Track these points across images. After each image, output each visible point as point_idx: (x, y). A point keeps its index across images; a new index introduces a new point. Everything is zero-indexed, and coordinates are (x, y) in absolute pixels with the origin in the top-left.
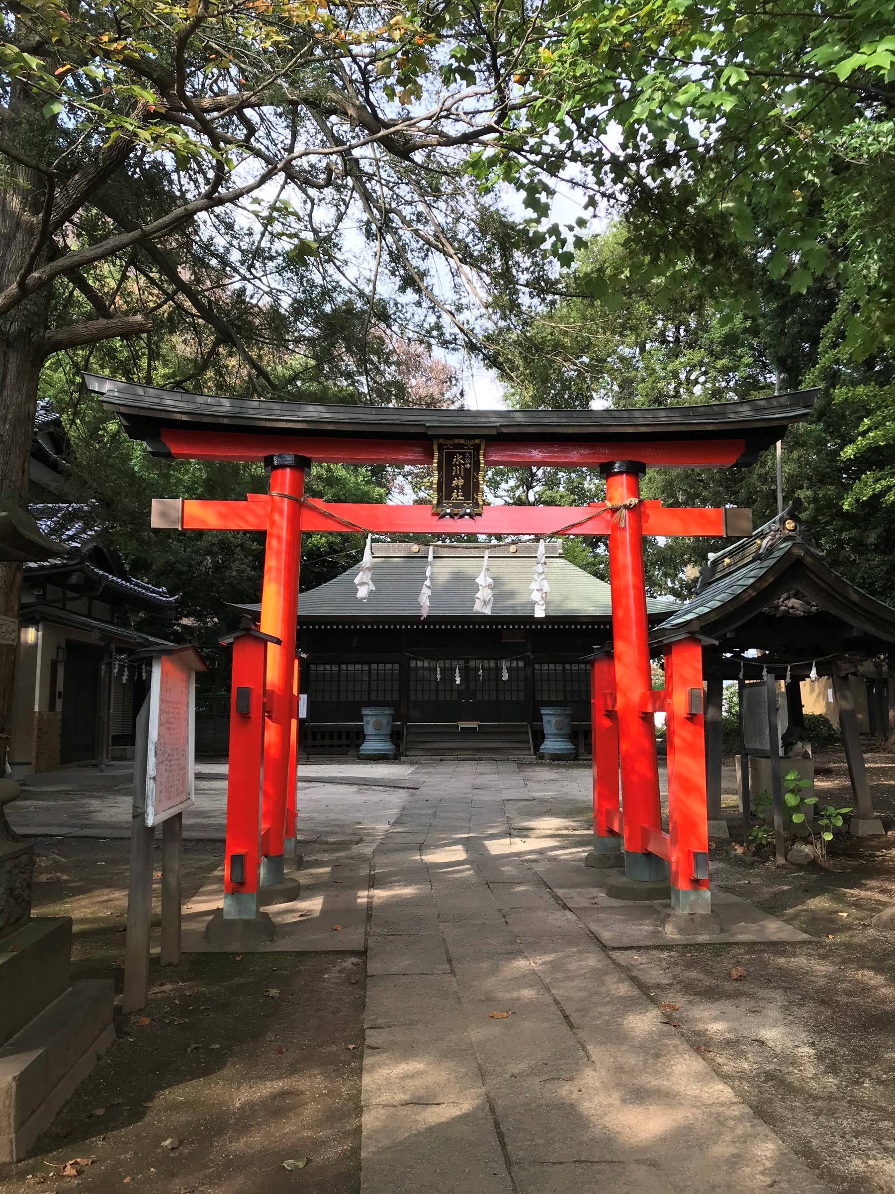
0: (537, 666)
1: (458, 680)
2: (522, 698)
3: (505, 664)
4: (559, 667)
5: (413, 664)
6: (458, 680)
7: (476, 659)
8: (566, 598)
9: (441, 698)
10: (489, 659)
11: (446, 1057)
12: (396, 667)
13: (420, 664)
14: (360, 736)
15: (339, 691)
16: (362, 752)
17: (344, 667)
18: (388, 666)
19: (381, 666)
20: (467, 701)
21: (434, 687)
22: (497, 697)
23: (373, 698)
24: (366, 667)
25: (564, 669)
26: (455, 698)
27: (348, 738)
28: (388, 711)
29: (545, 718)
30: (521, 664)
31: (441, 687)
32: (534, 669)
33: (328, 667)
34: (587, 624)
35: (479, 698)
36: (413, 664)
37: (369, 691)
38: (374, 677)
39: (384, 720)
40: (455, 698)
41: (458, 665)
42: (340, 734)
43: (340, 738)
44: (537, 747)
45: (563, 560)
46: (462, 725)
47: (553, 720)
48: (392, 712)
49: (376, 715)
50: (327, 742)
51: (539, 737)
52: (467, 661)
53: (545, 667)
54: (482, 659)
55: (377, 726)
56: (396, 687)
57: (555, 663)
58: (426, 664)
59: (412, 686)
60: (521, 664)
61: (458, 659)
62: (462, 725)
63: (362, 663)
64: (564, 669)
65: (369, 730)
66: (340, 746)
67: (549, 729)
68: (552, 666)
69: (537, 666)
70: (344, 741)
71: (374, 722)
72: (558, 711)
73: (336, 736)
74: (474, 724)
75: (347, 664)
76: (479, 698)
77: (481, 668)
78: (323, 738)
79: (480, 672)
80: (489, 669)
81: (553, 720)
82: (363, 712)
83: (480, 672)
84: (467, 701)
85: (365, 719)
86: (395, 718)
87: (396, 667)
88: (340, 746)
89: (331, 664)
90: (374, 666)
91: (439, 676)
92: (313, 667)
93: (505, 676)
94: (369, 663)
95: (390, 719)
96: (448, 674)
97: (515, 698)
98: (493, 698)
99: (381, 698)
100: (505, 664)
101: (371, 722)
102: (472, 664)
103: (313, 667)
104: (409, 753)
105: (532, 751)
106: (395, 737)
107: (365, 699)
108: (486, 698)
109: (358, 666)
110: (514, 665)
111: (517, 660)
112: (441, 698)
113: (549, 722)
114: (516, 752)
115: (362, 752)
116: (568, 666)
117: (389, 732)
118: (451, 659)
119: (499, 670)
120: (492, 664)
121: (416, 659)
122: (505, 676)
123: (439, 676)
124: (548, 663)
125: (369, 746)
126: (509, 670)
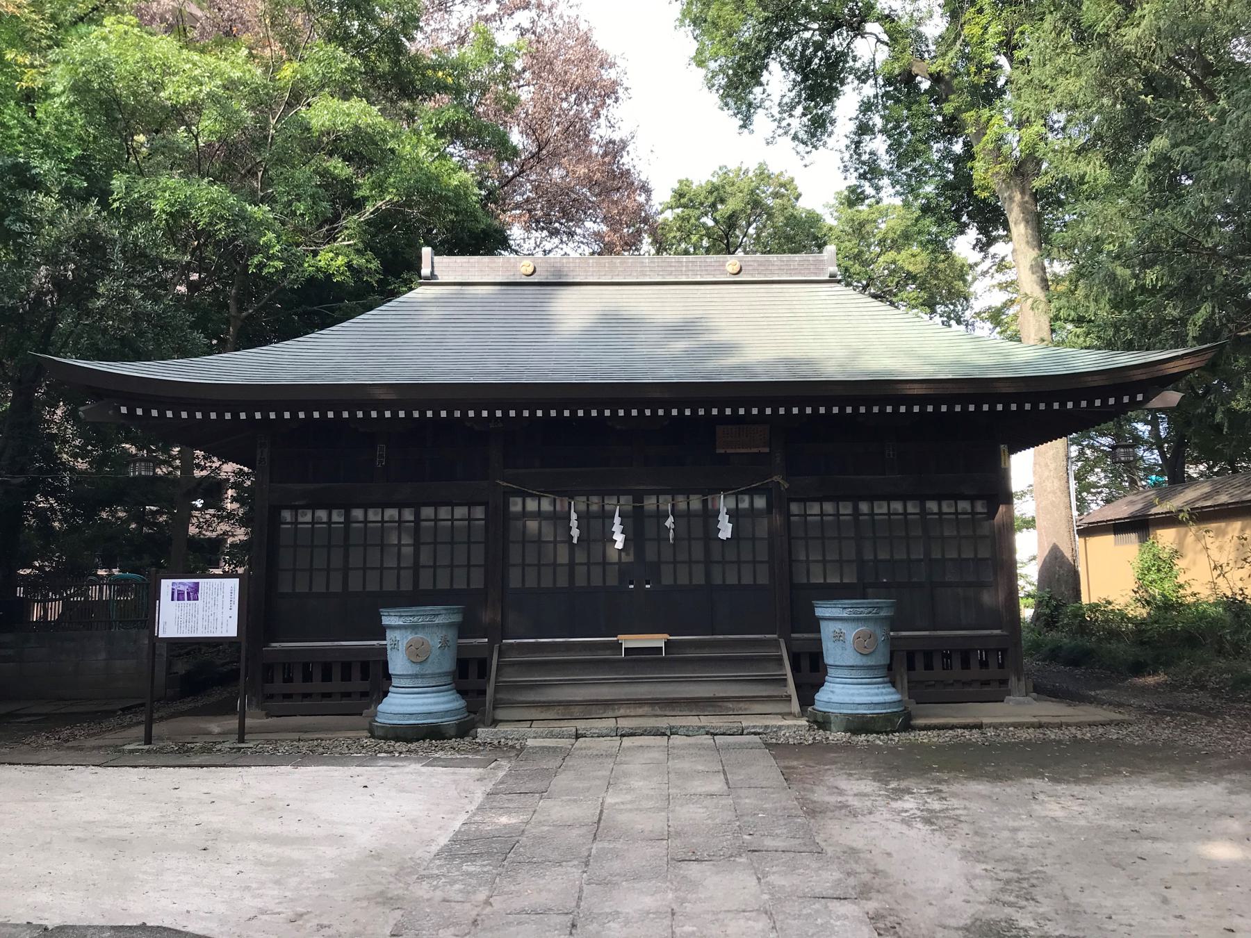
0: (795, 508)
1: (619, 539)
2: (763, 579)
3: (723, 504)
4: (846, 509)
5: (516, 505)
6: (619, 539)
7: (658, 493)
8: (857, 354)
9: (581, 581)
10: (688, 492)
11: (714, 189)
12: (479, 512)
13: (532, 505)
14: (373, 678)
15: (346, 570)
16: (380, 720)
17: (358, 513)
18: (460, 512)
19: (444, 512)
20: (639, 587)
21: (563, 558)
22: (708, 575)
23: (426, 583)
24: (408, 515)
25: (856, 512)
26: (612, 581)
27: (365, 676)
28: (445, 616)
29: (827, 629)
30: (760, 503)
31: (580, 557)
32: (789, 515)
33: (322, 514)
34: (923, 400)
35: (667, 580)
36: (516, 505)
37: (416, 567)
38: (426, 537)
39: (434, 640)
40: (612, 581)
41: (617, 507)
42: (346, 668)
43: (346, 677)
44: (807, 700)
45: (839, 288)
46: (630, 641)
47: (851, 632)
48: (457, 618)
49: (414, 628)
50: (317, 686)
51: (811, 670)
52: (638, 497)
53: (814, 509)
54: (673, 492)
55: (417, 654)
56: (478, 555)
57: (836, 499)
58: (546, 505)
59: (515, 555)
60: (760, 503)
61: (619, 493)
62: (630, 641)
63: (400, 506)
64: (856, 512)
65: (398, 663)
66: (347, 695)
67: (833, 653)
68: (829, 507)
69: (795, 508)
70: (336, 685)
71: (411, 644)
72: (862, 608)
73: (337, 672)
74: (657, 641)
75: (366, 507)
76: (667, 580)
77: (671, 511)
78: (327, 677)
79: (669, 522)
80: (688, 514)
81: (851, 632)
82: (819, 612)
83: (669, 522)
84: (639, 587)
85: (389, 634)
86: (464, 629)
87: (479, 512)
88: (347, 695)
89: (329, 507)
90: (427, 512)
91: (575, 533)
92: (287, 515)
93: (725, 530)
94: (417, 506)
95: (451, 635)
96: (596, 527)
97: (747, 580)
98: (699, 579)
99: (443, 584)
100: (723, 504)
101: (402, 645)
102: (650, 503)
103: (287, 515)
104: (501, 714)
105: (795, 706)
106: (468, 676)
107: (407, 586)
108: (683, 580)
109: (391, 513)
110: (745, 504)
111: (752, 492)
112: (581, 581)
113: (839, 637)
114: (758, 708)
115: (380, 720)
116: (864, 507)
117: (448, 665)
118: (603, 494)
119: (711, 517)
120: (696, 503)
121: (524, 495)
122: (725, 530)
123: (575, 533)
124: (821, 500)
125: (401, 705)
126: (734, 515)
